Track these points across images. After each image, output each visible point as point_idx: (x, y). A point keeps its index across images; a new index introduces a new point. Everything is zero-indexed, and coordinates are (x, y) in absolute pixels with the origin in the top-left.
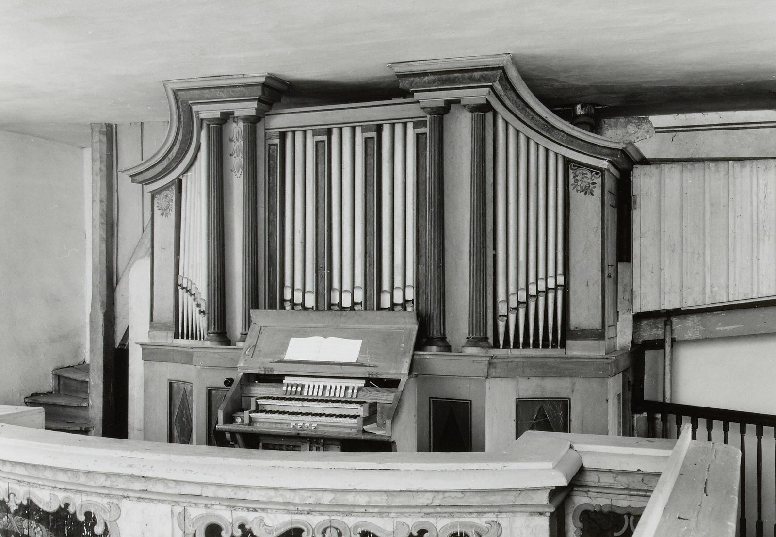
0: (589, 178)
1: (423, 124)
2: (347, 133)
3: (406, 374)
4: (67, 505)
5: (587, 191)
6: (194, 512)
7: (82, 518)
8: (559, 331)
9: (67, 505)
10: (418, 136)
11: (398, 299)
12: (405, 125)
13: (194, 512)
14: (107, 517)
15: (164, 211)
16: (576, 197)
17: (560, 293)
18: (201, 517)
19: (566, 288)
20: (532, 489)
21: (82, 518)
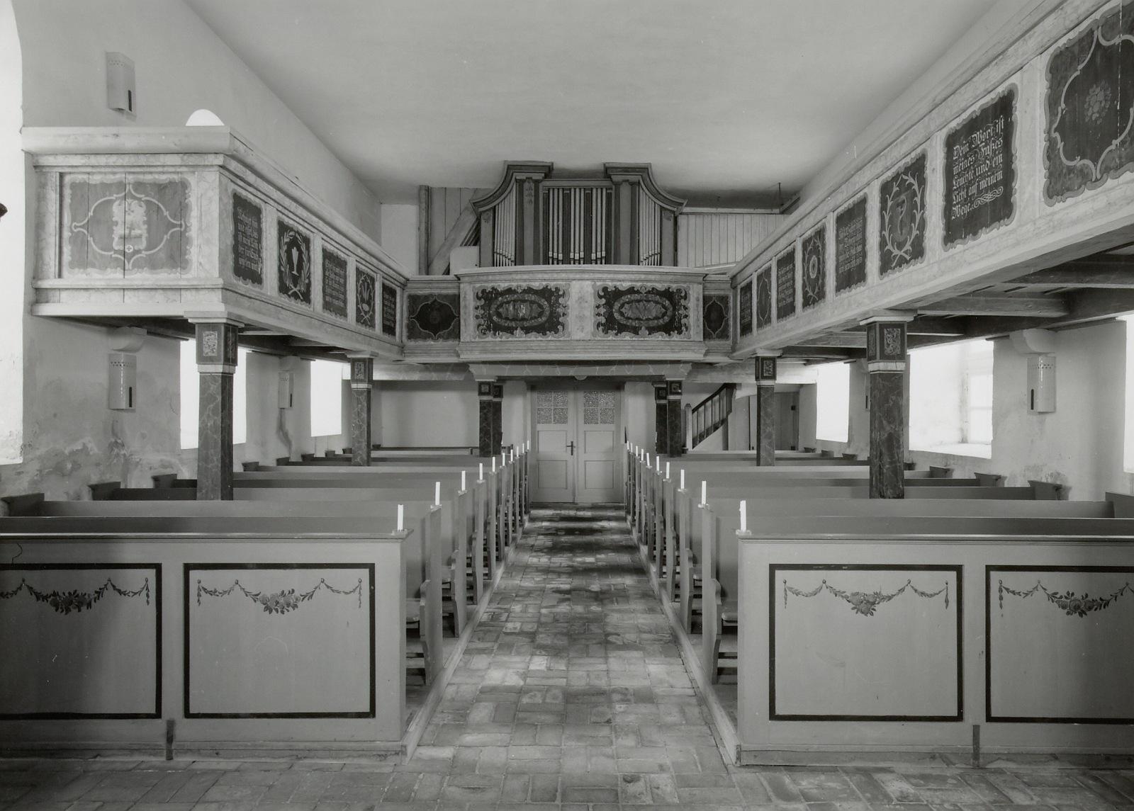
0: (669, 214)
1: (611, 189)
2: (578, 190)
3: (125, 477)
4: (547, 286)
5: (669, 219)
6: (598, 283)
7: (554, 290)
8: (152, 534)
9: (547, 286)
10: (607, 194)
11: (599, 256)
12: (602, 189)
13: (598, 283)
14: (564, 288)
15: (487, 221)
16: (665, 220)
17: (659, 255)
18: (601, 285)
19: (661, 254)
20: (581, 373)
21: (554, 290)
